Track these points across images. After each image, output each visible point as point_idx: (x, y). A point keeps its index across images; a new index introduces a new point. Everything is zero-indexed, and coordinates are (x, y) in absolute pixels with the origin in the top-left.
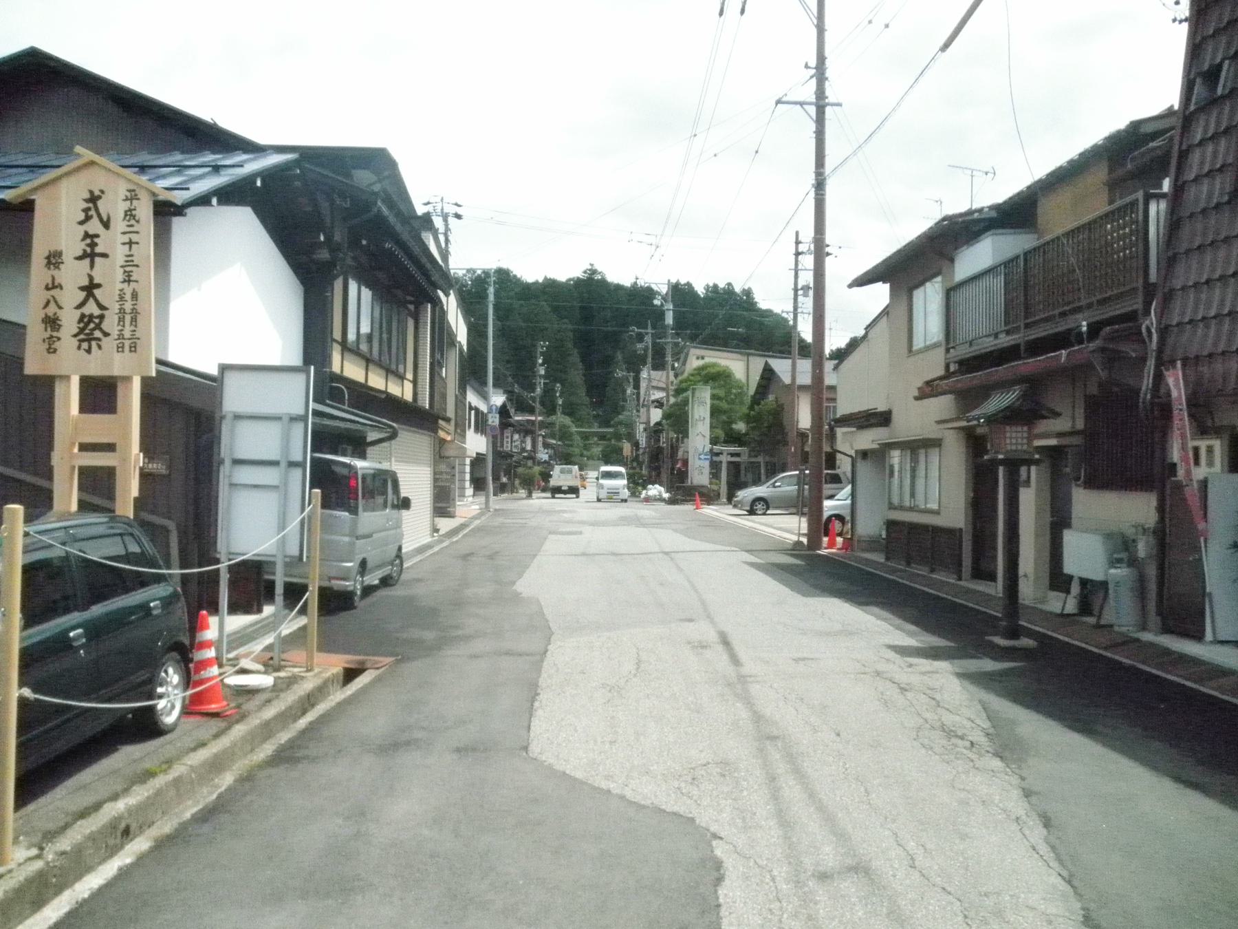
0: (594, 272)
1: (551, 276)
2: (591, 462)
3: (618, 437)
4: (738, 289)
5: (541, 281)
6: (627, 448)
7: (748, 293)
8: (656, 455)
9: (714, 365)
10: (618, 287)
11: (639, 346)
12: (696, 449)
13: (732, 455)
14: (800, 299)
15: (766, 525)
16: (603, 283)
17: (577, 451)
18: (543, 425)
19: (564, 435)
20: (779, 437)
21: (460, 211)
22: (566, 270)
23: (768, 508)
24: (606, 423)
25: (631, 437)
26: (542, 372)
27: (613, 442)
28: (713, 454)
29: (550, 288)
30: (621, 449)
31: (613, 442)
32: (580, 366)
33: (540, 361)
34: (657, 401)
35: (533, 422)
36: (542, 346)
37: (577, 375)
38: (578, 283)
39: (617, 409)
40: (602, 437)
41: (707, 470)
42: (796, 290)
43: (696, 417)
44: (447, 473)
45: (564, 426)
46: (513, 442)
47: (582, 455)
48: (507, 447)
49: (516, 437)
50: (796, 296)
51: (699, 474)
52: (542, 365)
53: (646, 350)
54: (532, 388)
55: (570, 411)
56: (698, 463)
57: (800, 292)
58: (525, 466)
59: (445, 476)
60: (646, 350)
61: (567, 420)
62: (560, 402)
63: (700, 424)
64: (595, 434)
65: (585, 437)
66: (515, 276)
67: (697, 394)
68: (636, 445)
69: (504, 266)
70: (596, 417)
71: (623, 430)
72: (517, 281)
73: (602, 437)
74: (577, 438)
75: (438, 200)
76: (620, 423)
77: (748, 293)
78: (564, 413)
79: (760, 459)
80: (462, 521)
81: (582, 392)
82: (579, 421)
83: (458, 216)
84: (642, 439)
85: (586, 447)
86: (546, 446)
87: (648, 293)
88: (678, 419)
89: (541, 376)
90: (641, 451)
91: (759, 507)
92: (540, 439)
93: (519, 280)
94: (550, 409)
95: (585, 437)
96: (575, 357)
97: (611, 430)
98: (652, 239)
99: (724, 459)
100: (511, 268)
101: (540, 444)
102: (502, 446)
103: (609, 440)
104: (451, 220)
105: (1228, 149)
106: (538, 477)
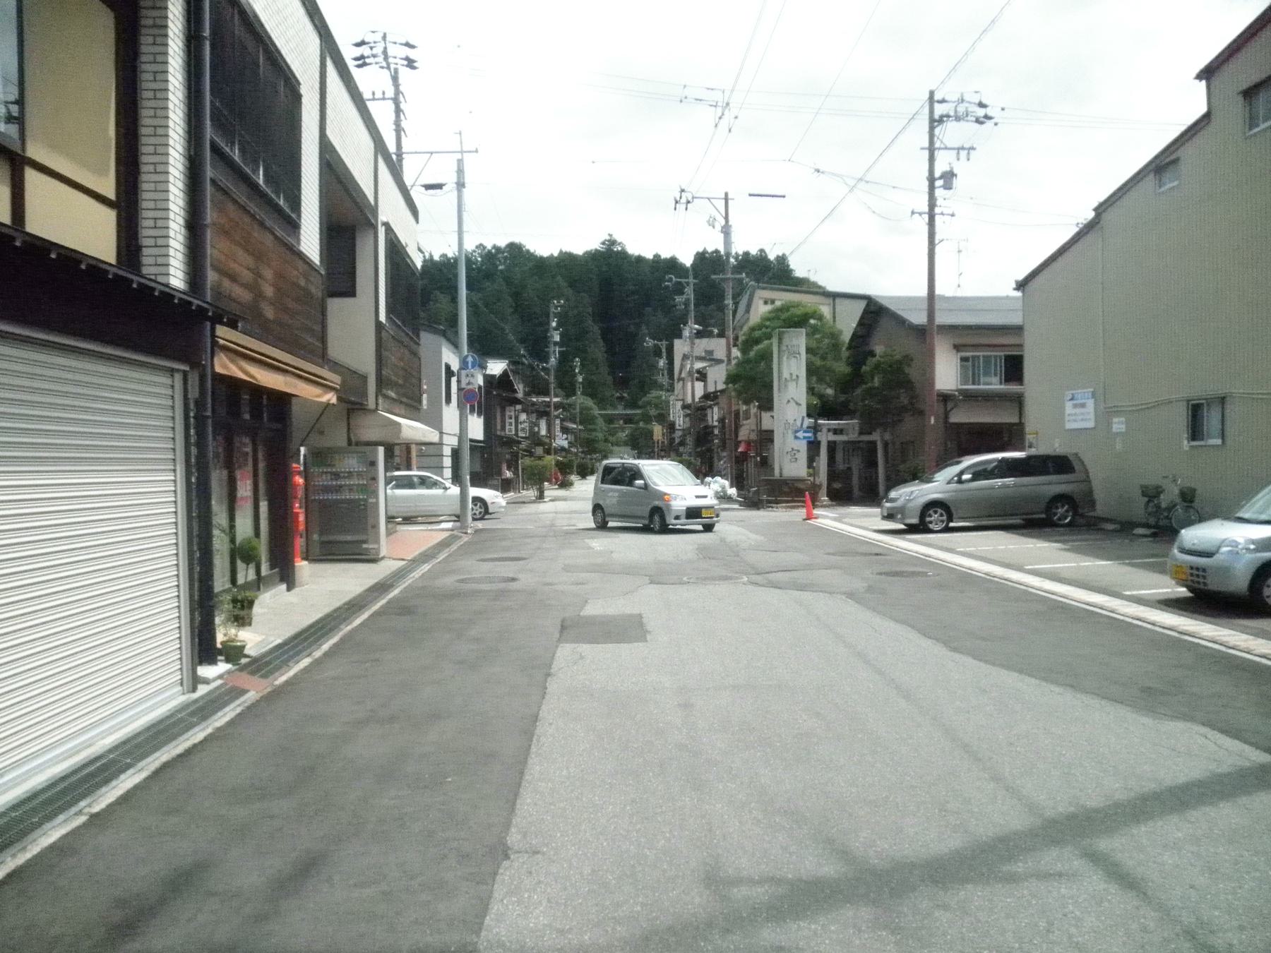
0: (613, 242)
1: (566, 249)
2: (616, 449)
3: (647, 419)
4: (772, 257)
5: (556, 254)
6: (658, 431)
7: (782, 260)
8: (703, 436)
9: (798, 305)
10: (640, 259)
11: (678, 299)
12: (787, 423)
13: (836, 431)
14: (939, 193)
15: (852, 525)
16: (623, 255)
17: (600, 436)
18: (557, 406)
19: (587, 419)
20: (904, 400)
21: (412, 54)
22: (582, 242)
23: (950, 519)
24: (633, 404)
25: (662, 418)
26: (557, 338)
27: (641, 424)
28: (815, 429)
29: (566, 262)
30: (651, 433)
31: (641, 424)
32: (601, 343)
33: (554, 324)
34: (698, 372)
35: (548, 405)
36: (556, 305)
37: (598, 351)
38: (594, 256)
39: (646, 385)
40: (629, 420)
41: (803, 456)
42: (932, 180)
43: (786, 375)
44: (359, 474)
45: (584, 409)
46: (517, 423)
47: (606, 441)
48: (510, 430)
49: (523, 417)
50: (932, 188)
51: (791, 460)
52: (556, 329)
53: (687, 304)
54: (545, 358)
55: (591, 390)
56: (792, 443)
57: (939, 183)
58: (531, 454)
59: (354, 481)
60: (687, 304)
61: (589, 402)
62: (580, 379)
63: (792, 386)
64: (620, 416)
65: (610, 420)
66: (528, 251)
67: (786, 341)
68: (672, 427)
69: (517, 240)
70: (621, 398)
71: (653, 412)
72: (530, 256)
73: (629, 420)
74: (600, 422)
75: (378, 37)
76: (649, 403)
77: (782, 260)
78: (583, 394)
79: (876, 436)
80: (394, 565)
81: (604, 370)
82: (602, 402)
83: (411, 63)
84: (679, 418)
85: (613, 433)
86: (565, 430)
87: (672, 265)
88: (754, 383)
89: (556, 344)
90: (678, 434)
91: (935, 518)
92: (558, 421)
93: (532, 255)
94: (567, 387)
95: (610, 420)
96: (595, 329)
97: (638, 411)
98: (717, 96)
99: (824, 438)
100: (523, 242)
101: (558, 428)
102: (503, 428)
103: (637, 423)
104: (404, 73)
105: (447, 530)
106: (554, 469)
